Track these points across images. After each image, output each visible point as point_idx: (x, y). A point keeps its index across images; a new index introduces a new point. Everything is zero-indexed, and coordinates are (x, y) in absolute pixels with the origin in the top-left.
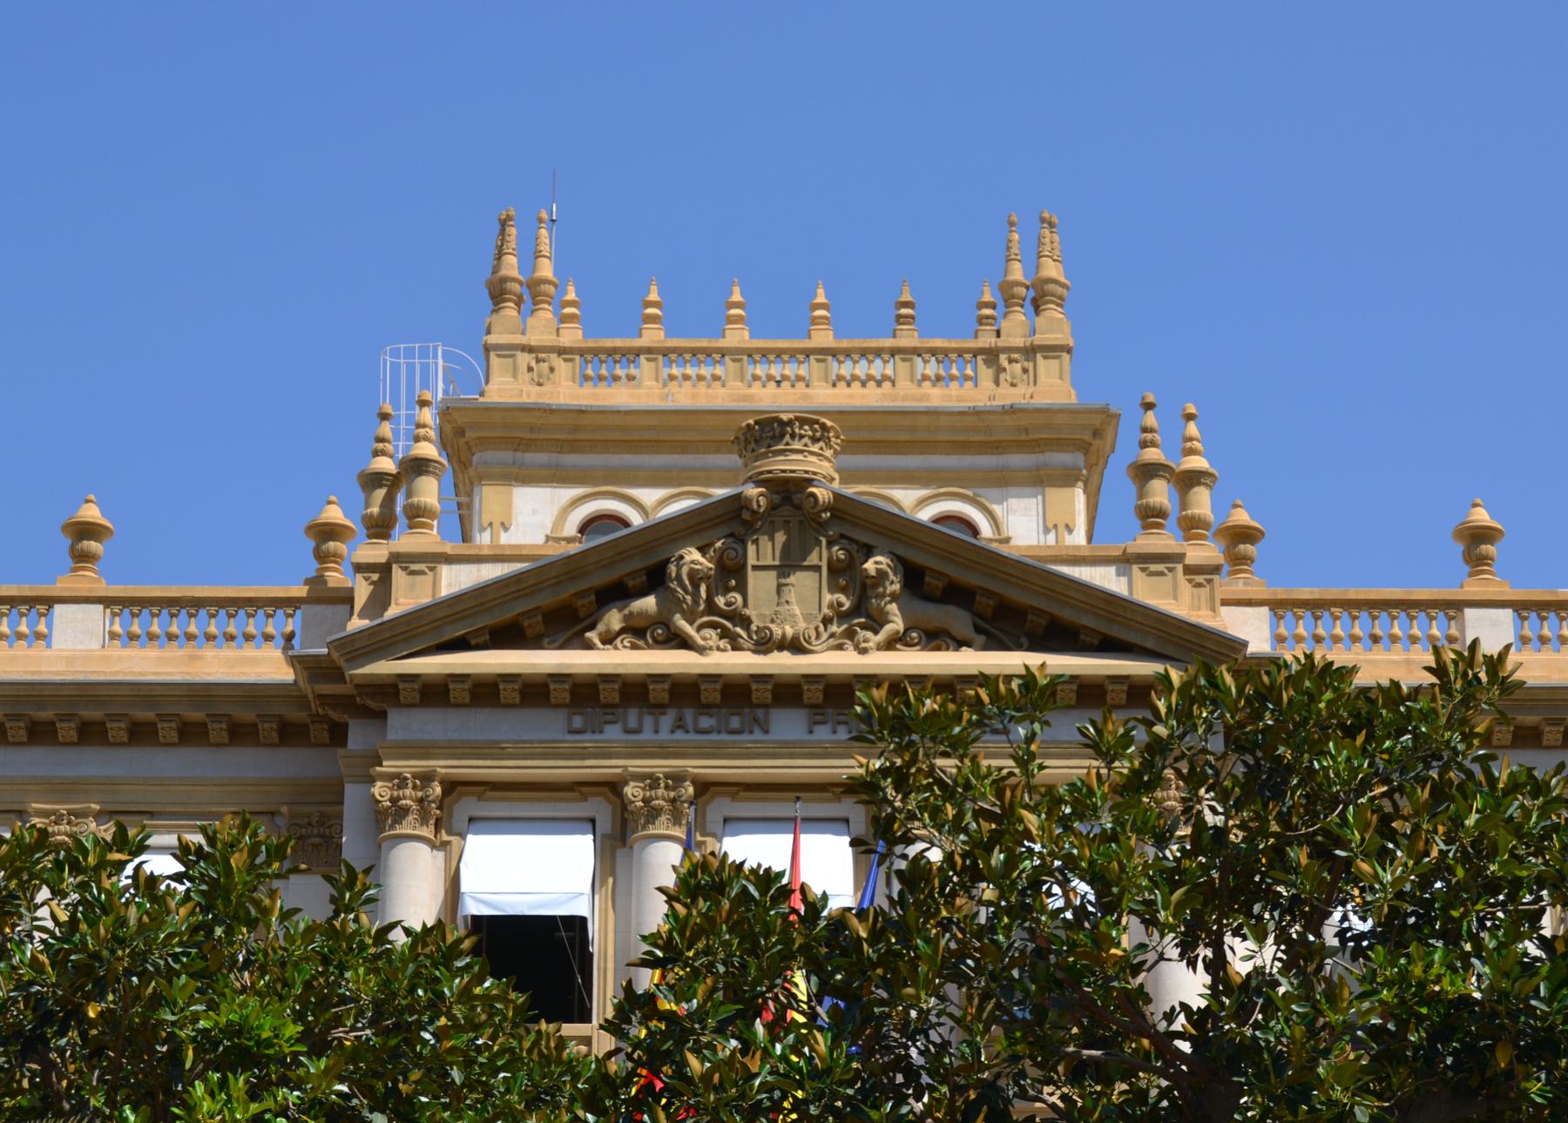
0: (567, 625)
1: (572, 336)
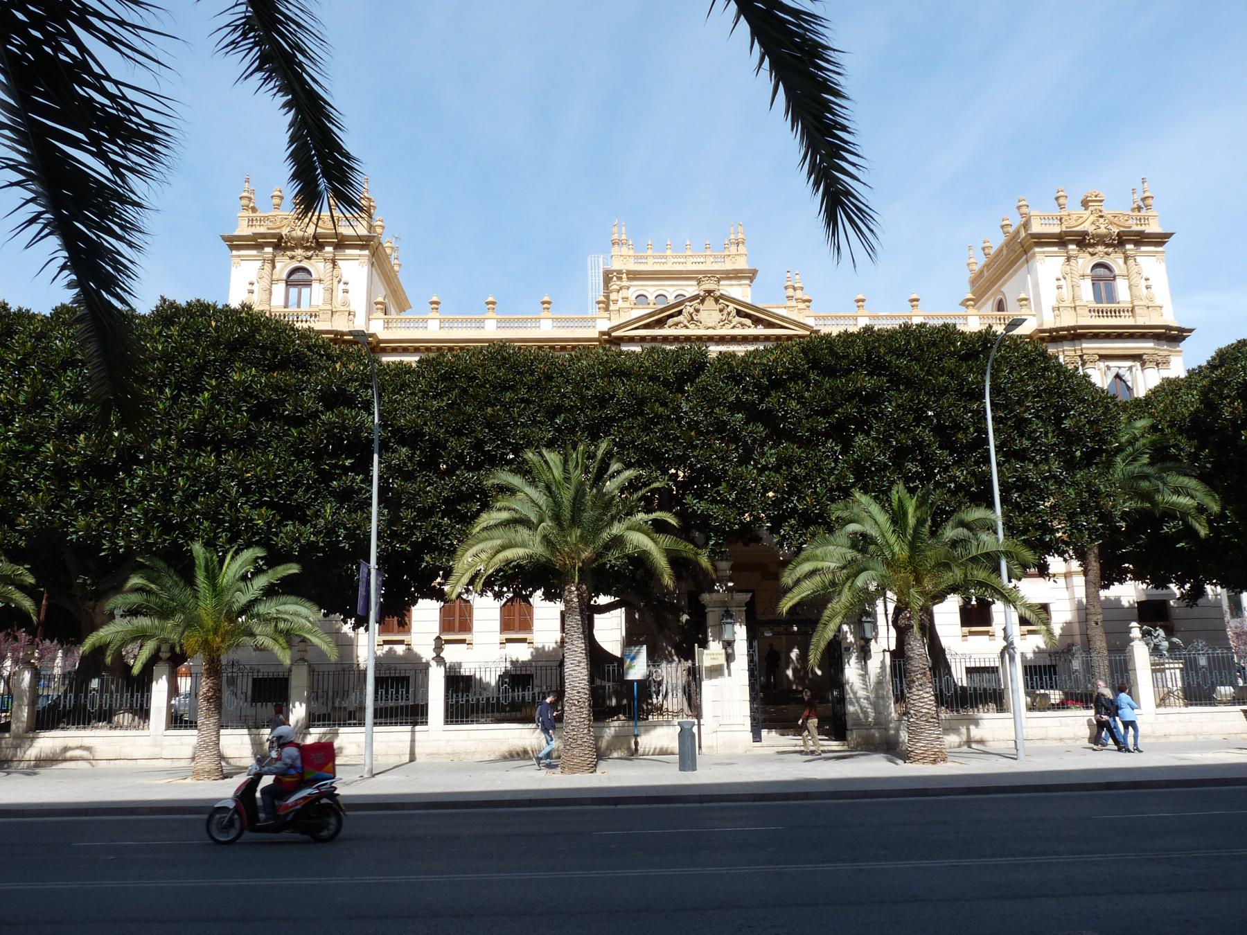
0: (660, 323)
1: (631, 253)
